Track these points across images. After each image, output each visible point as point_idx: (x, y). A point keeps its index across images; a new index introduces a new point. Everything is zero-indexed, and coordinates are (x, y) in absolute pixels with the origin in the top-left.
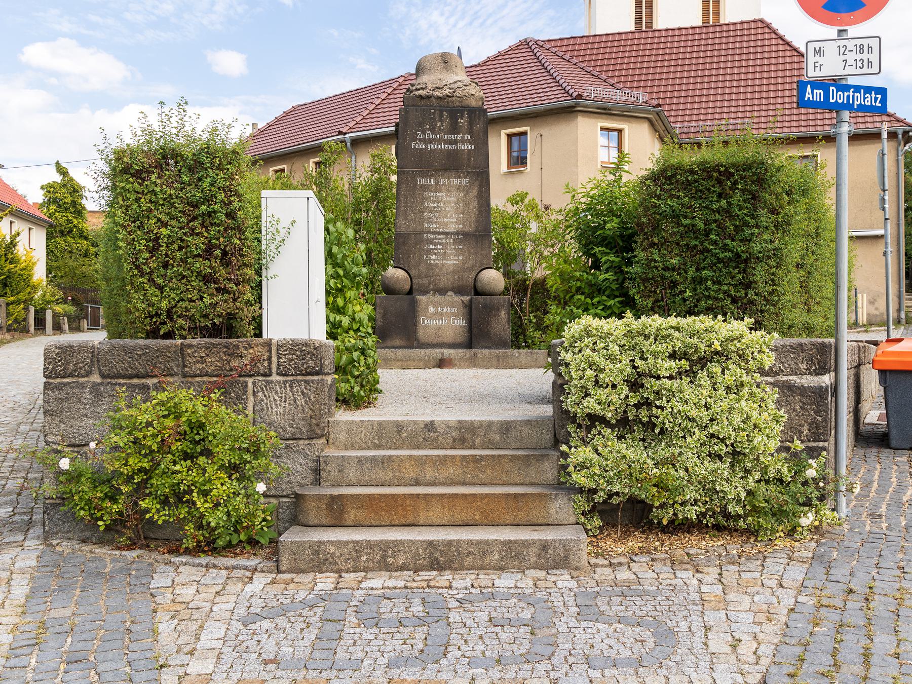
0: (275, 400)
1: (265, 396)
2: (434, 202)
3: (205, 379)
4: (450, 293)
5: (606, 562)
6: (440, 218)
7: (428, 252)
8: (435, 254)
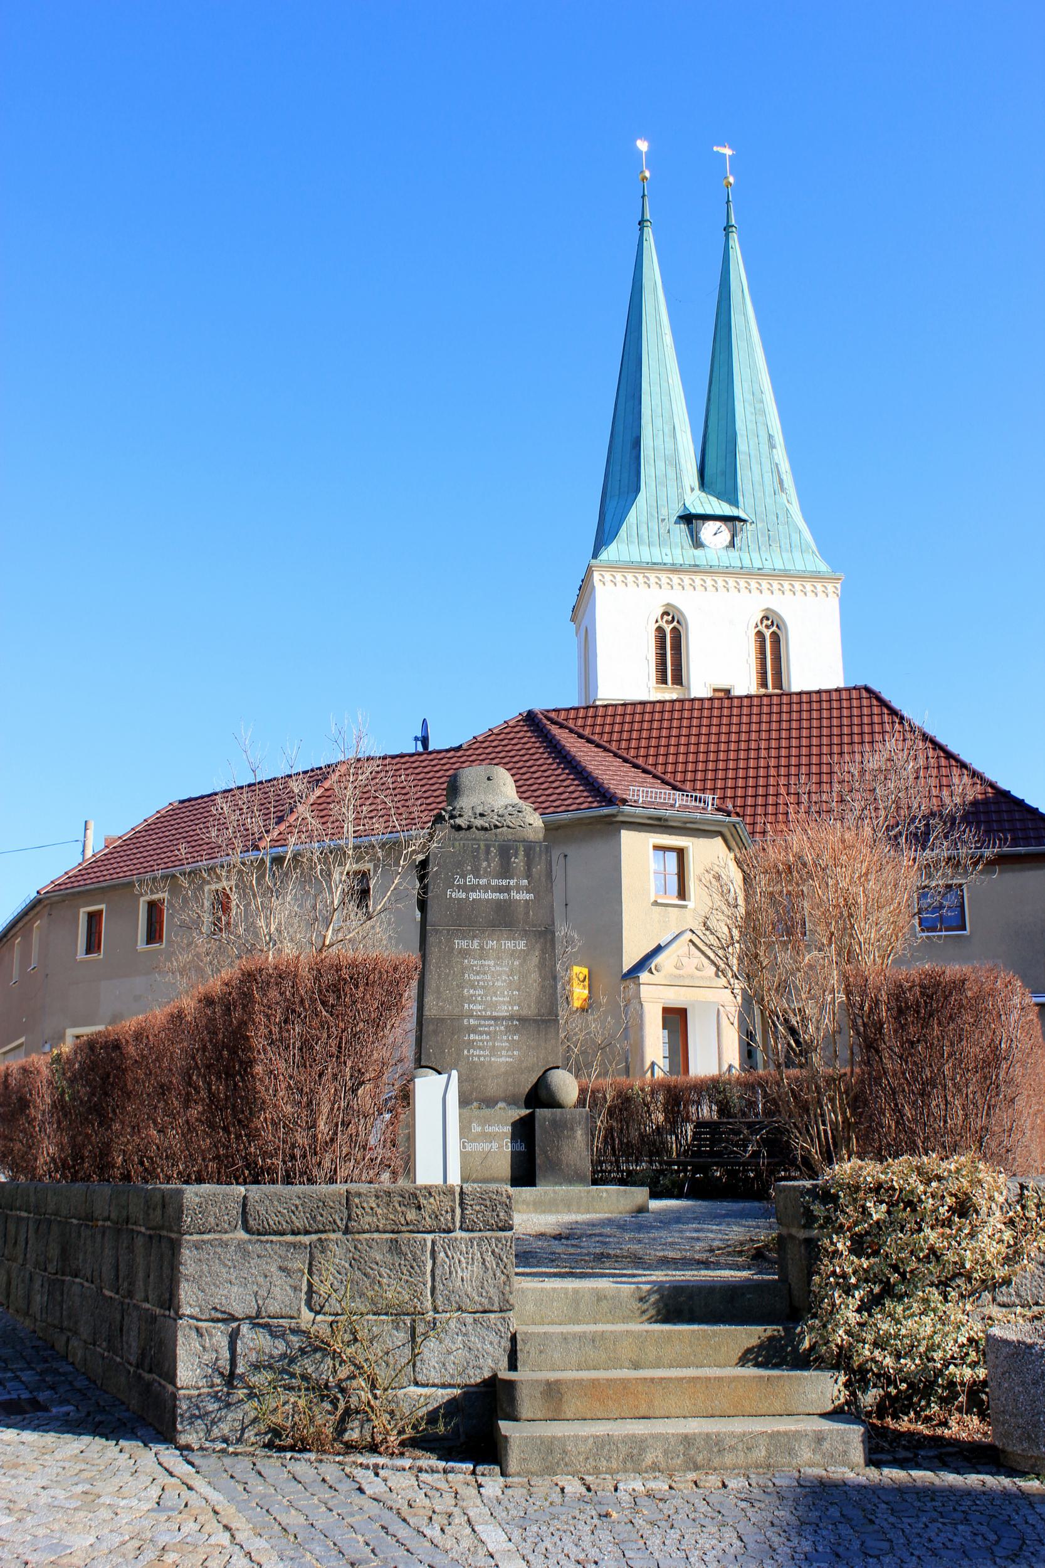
0: (459, 1262)
1: (448, 1257)
2: (478, 973)
3: (376, 1235)
4: (501, 1105)
5: (890, 1458)
6: (486, 996)
7: (470, 1044)
8: (480, 1048)
